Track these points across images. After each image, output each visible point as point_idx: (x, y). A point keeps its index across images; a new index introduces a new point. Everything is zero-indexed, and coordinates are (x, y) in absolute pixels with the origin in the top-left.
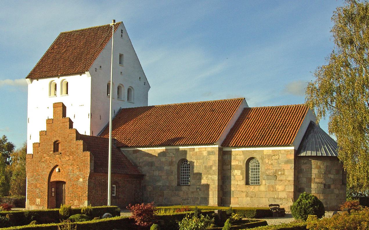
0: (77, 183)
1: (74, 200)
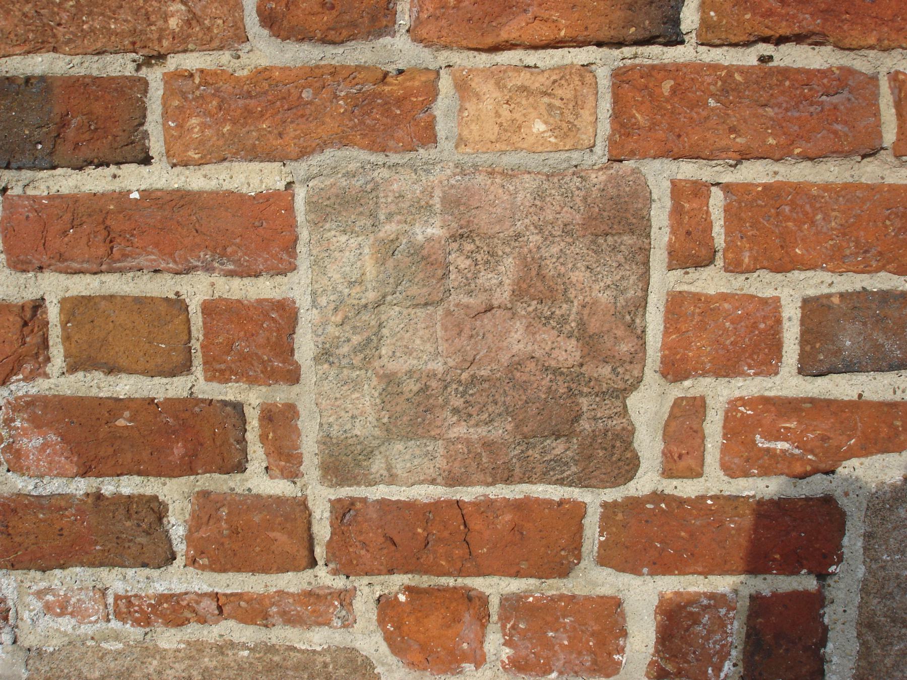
1: (260, 116)
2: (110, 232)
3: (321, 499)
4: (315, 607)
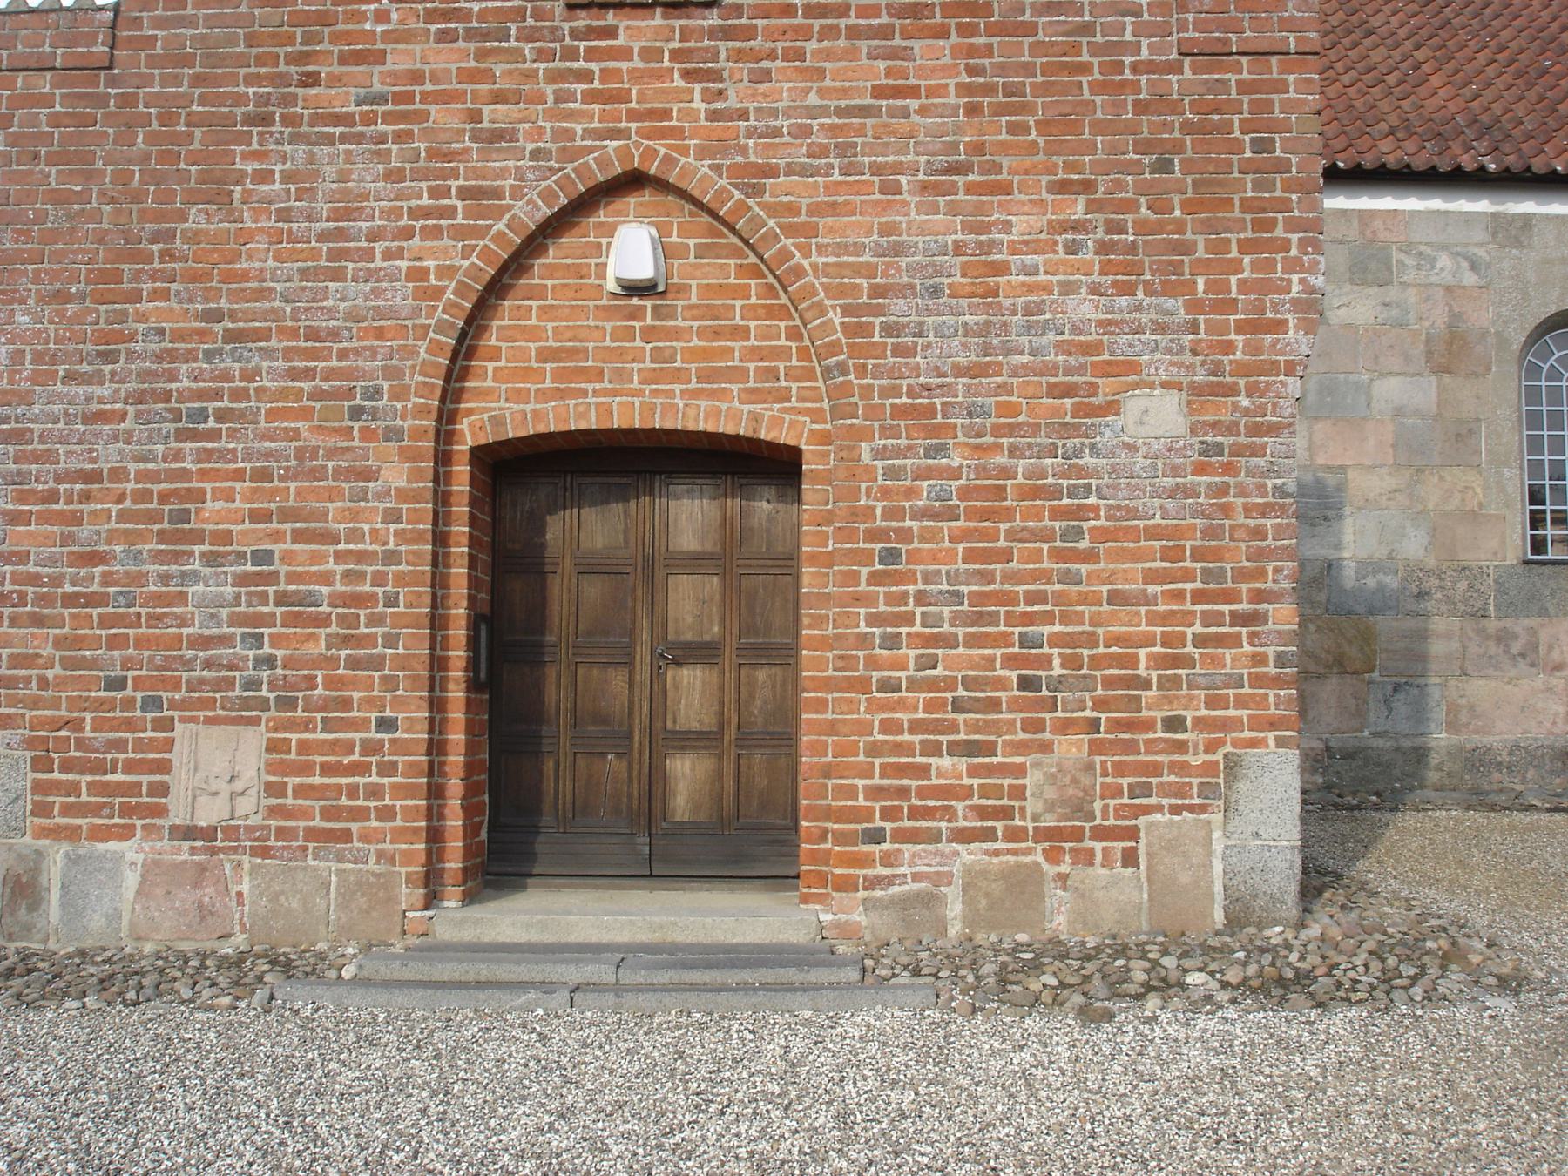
0: (1082, 472)
1: (1021, 748)
2: (990, 770)
3: (1030, 826)
4: (1028, 852)
